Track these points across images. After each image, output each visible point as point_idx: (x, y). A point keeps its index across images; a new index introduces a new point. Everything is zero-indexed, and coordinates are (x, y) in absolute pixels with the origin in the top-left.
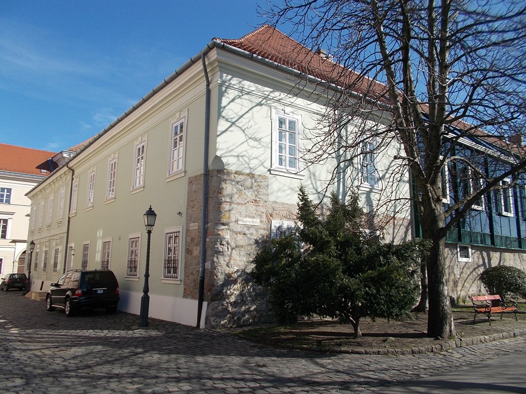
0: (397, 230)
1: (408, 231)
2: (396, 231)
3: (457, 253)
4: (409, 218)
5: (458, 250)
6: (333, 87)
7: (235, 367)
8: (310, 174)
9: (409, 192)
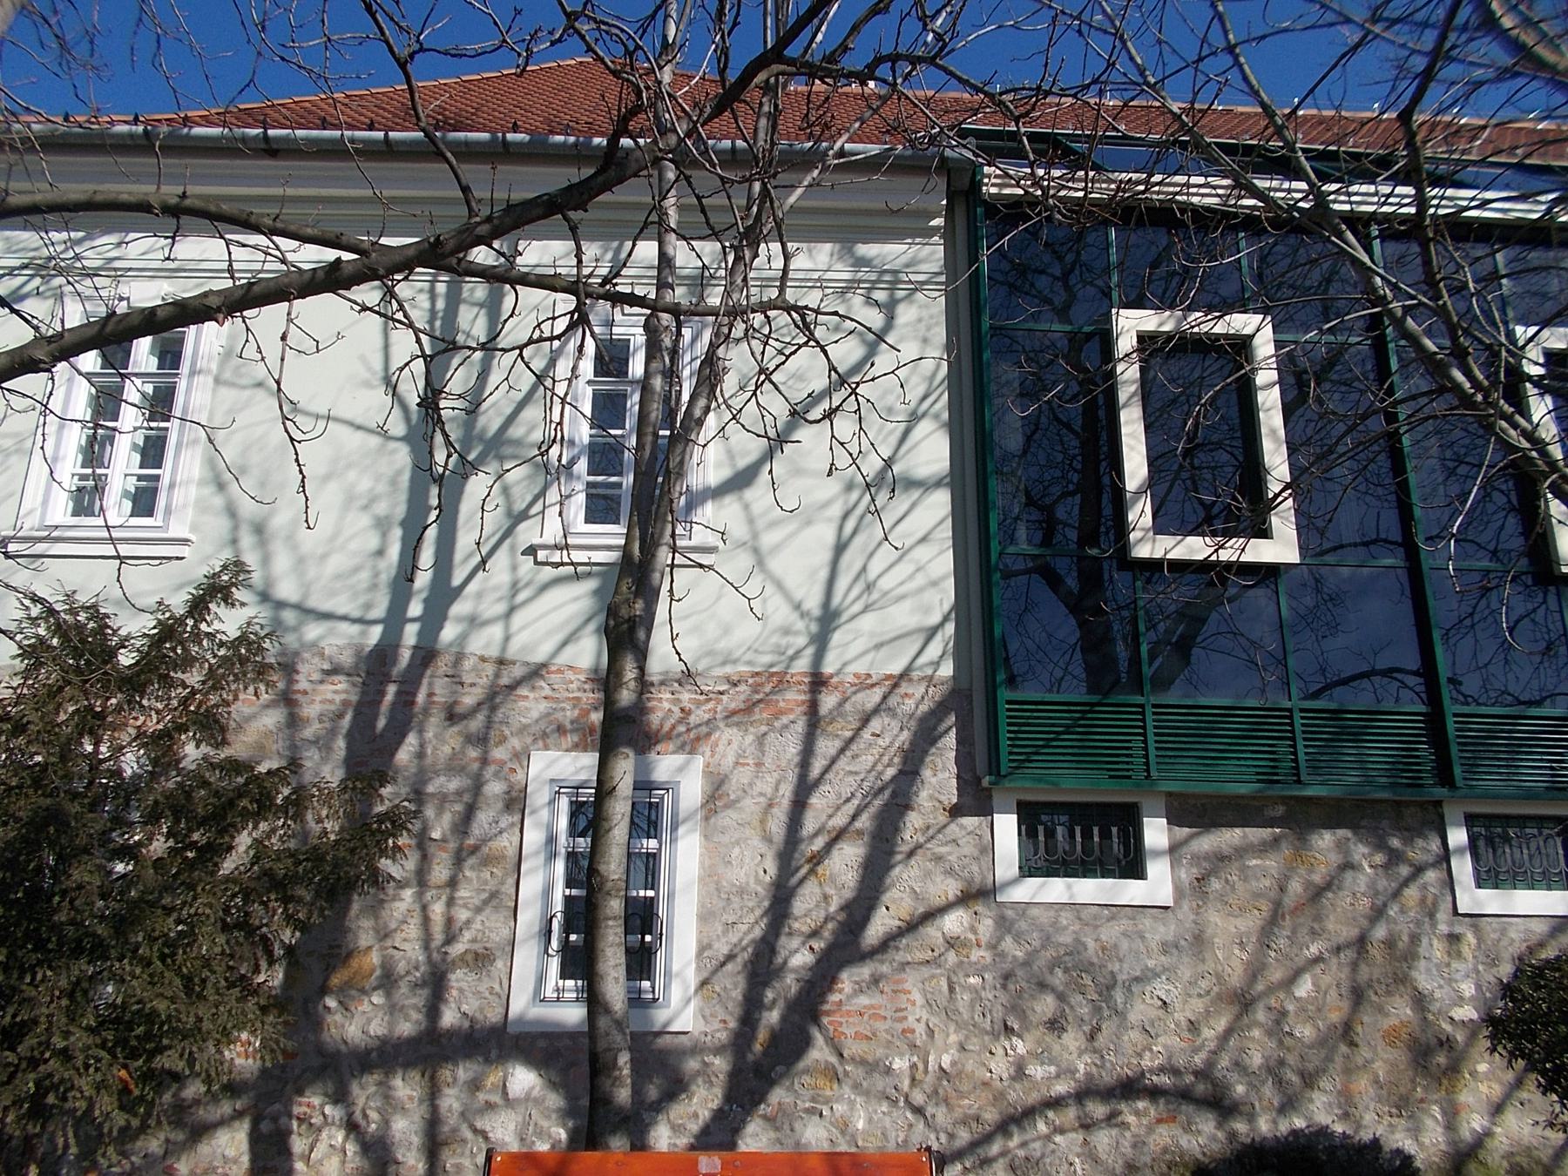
0: (838, 744)
1: (933, 741)
2: (826, 747)
3: (1445, 857)
4: (947, 670)
5: (1458, 836)
6: (520, 144)
7: (1504, 1053)
8: (236, 528)
9: (946, 531)
